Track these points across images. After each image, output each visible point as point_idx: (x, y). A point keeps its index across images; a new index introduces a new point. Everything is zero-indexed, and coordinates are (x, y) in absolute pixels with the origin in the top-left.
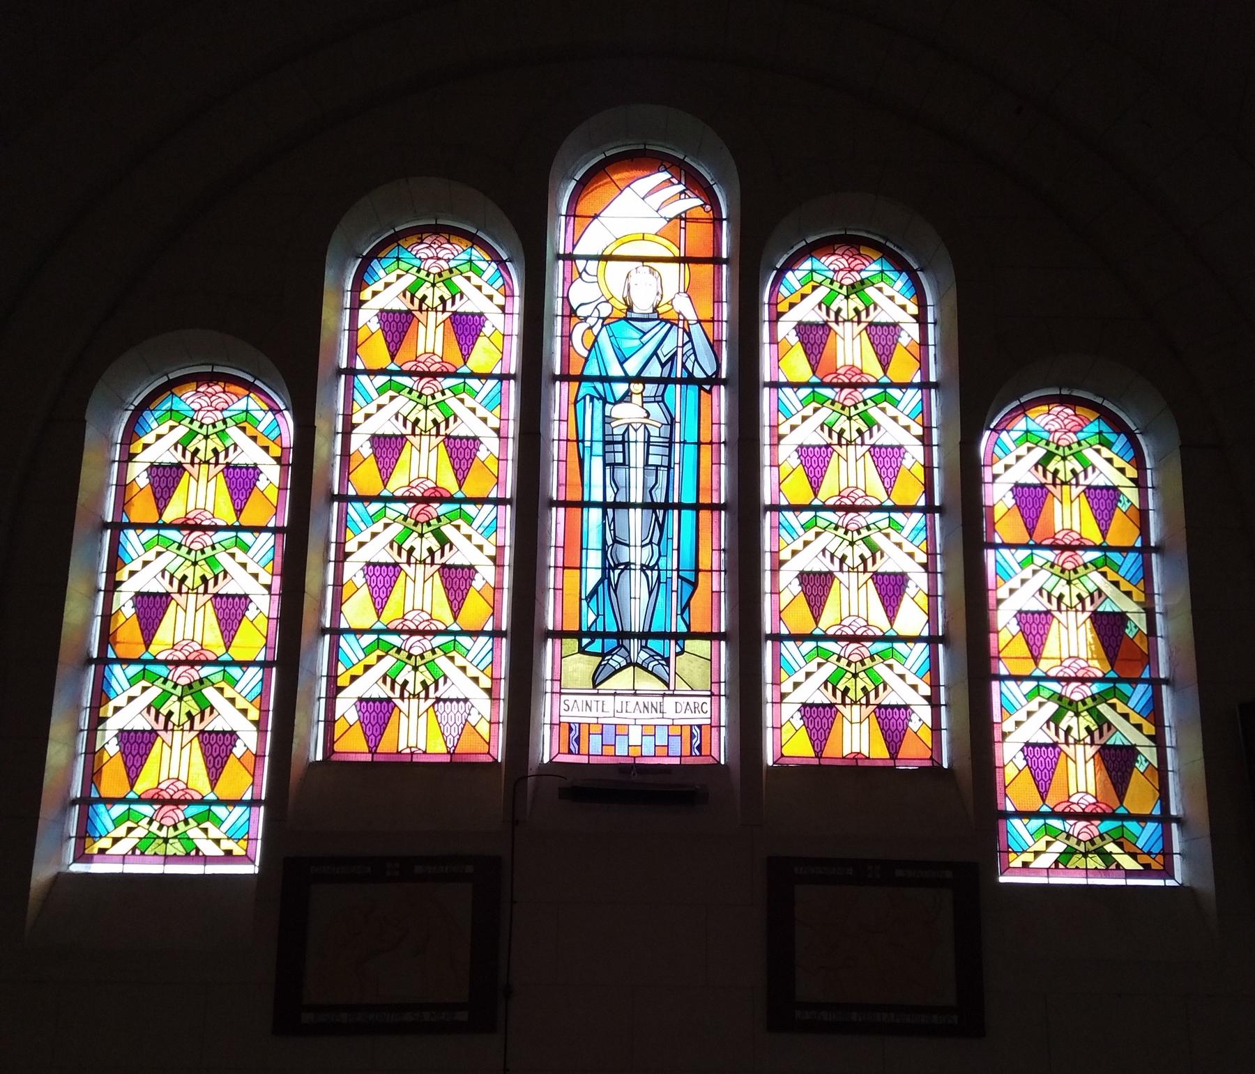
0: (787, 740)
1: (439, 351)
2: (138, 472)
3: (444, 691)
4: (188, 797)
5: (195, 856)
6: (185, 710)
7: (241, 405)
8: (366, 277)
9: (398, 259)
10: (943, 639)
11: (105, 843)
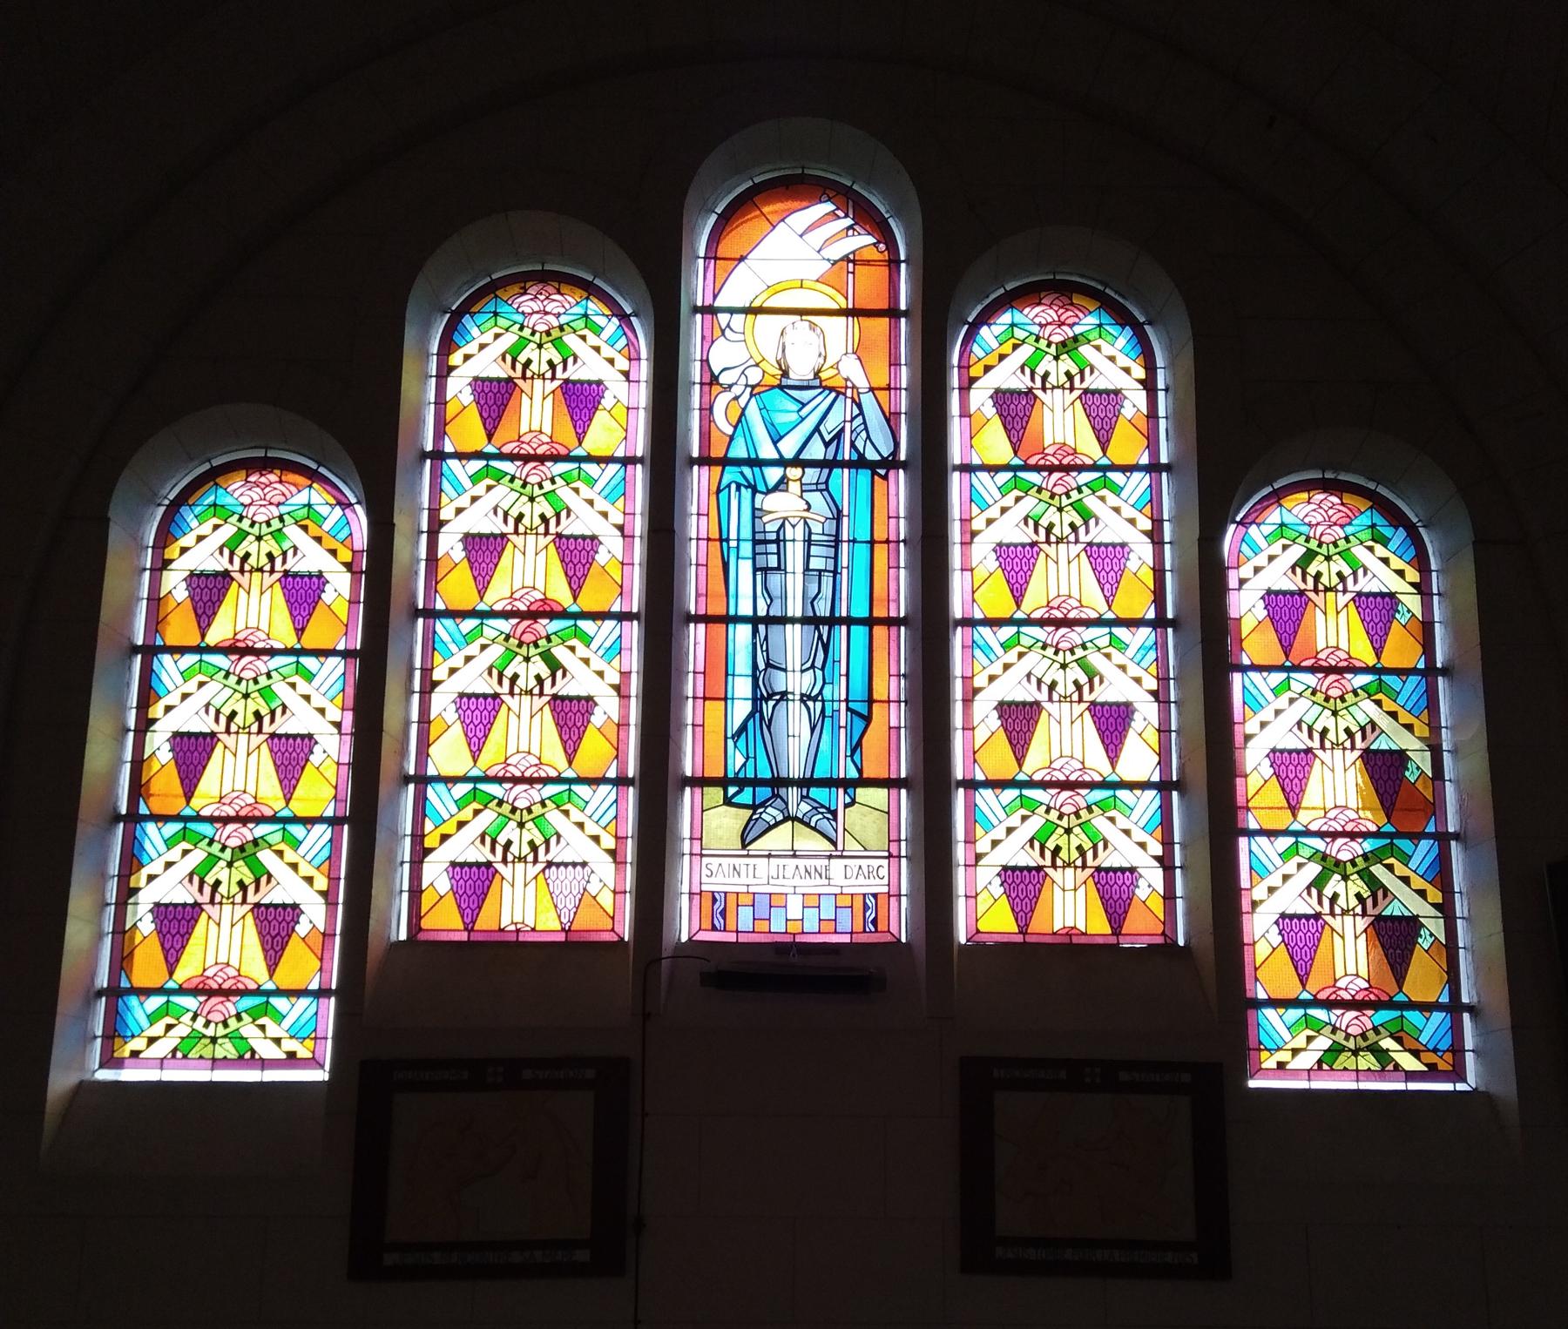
0: (983, 912)
1: (547, 429)
2: (174, 583)
3: (557, 853)
4: (241, 986)
5: (250, 1059)
6: (236, 878)
7: (302, 498)
8: (456, 337)
9: (496, 314)
10: (1179, 785)
11: (138, 1044)
